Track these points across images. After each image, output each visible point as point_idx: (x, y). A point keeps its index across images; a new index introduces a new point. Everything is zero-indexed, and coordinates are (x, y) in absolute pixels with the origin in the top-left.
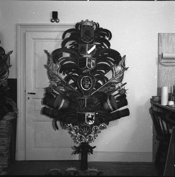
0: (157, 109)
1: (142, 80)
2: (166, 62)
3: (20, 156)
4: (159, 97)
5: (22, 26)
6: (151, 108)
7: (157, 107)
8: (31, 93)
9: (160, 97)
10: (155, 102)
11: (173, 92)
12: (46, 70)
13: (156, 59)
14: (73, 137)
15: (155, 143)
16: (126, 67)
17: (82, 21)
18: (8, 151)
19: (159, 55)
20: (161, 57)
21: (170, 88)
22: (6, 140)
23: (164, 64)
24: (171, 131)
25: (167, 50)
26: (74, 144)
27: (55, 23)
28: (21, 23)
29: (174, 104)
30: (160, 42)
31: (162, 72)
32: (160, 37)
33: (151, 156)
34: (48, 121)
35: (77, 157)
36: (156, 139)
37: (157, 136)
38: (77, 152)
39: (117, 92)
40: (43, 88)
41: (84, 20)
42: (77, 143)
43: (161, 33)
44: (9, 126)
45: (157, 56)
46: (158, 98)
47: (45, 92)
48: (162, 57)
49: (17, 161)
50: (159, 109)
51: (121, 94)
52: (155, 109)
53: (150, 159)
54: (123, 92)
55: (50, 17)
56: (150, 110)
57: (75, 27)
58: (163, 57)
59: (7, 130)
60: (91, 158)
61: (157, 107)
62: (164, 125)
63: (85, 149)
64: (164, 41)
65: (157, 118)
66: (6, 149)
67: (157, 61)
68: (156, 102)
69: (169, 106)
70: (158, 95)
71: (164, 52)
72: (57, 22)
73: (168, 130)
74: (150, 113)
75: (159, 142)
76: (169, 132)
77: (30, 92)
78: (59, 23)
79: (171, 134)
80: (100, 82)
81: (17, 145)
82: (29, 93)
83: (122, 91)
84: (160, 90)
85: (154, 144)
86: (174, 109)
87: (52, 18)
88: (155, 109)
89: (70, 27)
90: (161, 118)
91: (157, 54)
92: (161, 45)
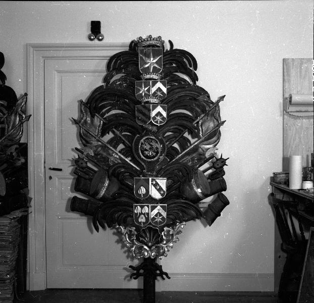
0: (282, 195)
1: (251, 146)
2: (298, 110)
3: (37, 281)
4: (286, 174)
5: (38, 47)
6: (272, 194)
7: (283, 192)
8: (54, 169)
9: (288, 174)
10: (280, 183)
11: (310, 165)
12: (74, 129)
13: (280, 105)
14: (126, 249)
15: (280, 257)
16: (222, 120)
17: (140, 38)
18: (13, 274)
19: (285, 99)
20: (288, 101)
21: (305, 157)
22: (10, 255)
23: (294, 114)
24: (307, 235)
25: (299, 88)
26: (129, 263)
27: (96, 41)
28: (36, 42)
29: (313, 186)
30: (286, 74)
31: (290, 130)
32: (286, 65)
33: (272, 280)
34: (80, 222)
35: (134, 284)
36: (280, 250)
37: (282, 244)
38: (135, 277)
39: (206, 165)
40: (69, 160)
41: (144, 37)
42: (133, 258)
43: (288, 59)
44: (14, 229)
45: (281, 101)
46: (284, 175)
47: (72, 167)
48: (290, 101)
49: (33, 292)
50: (285, 196)
51: (215, 168)
52: (279, 196)
53: (270, 287)
54: (220, 165)
55: (87, 30)
56: (269, 197)
57: (128, 48)
58: (292, 101)
59: (11, 237)
60: (161, 286)
61: (283, 192)
62: (294, 224)
63: (150, 271)
64: (293, 72)
65: (282, 213)
66: (8, 271)
67: (282, 109)
68: (280, 183)
69: (303, 190)
70: (283, 170)
71: (293, 92)
72: (100, 40)
73: (302, 233)
74: (270, 203)
75: (285, 255)
76: (303, 237)
77: (52, 167)
78: (104, 41)
79: (307, 240)
80: (176, 145)
81: (28, 264)
82: (50, 169)
83: (83, 163)
84: (287, 162)
85: (277, 258)
86: (313, 195)
87: (91, 33)
88: (279, 196)
89: (117, 48)
90: (289, 213)
91: (282, 97)
92: (289, 81)
